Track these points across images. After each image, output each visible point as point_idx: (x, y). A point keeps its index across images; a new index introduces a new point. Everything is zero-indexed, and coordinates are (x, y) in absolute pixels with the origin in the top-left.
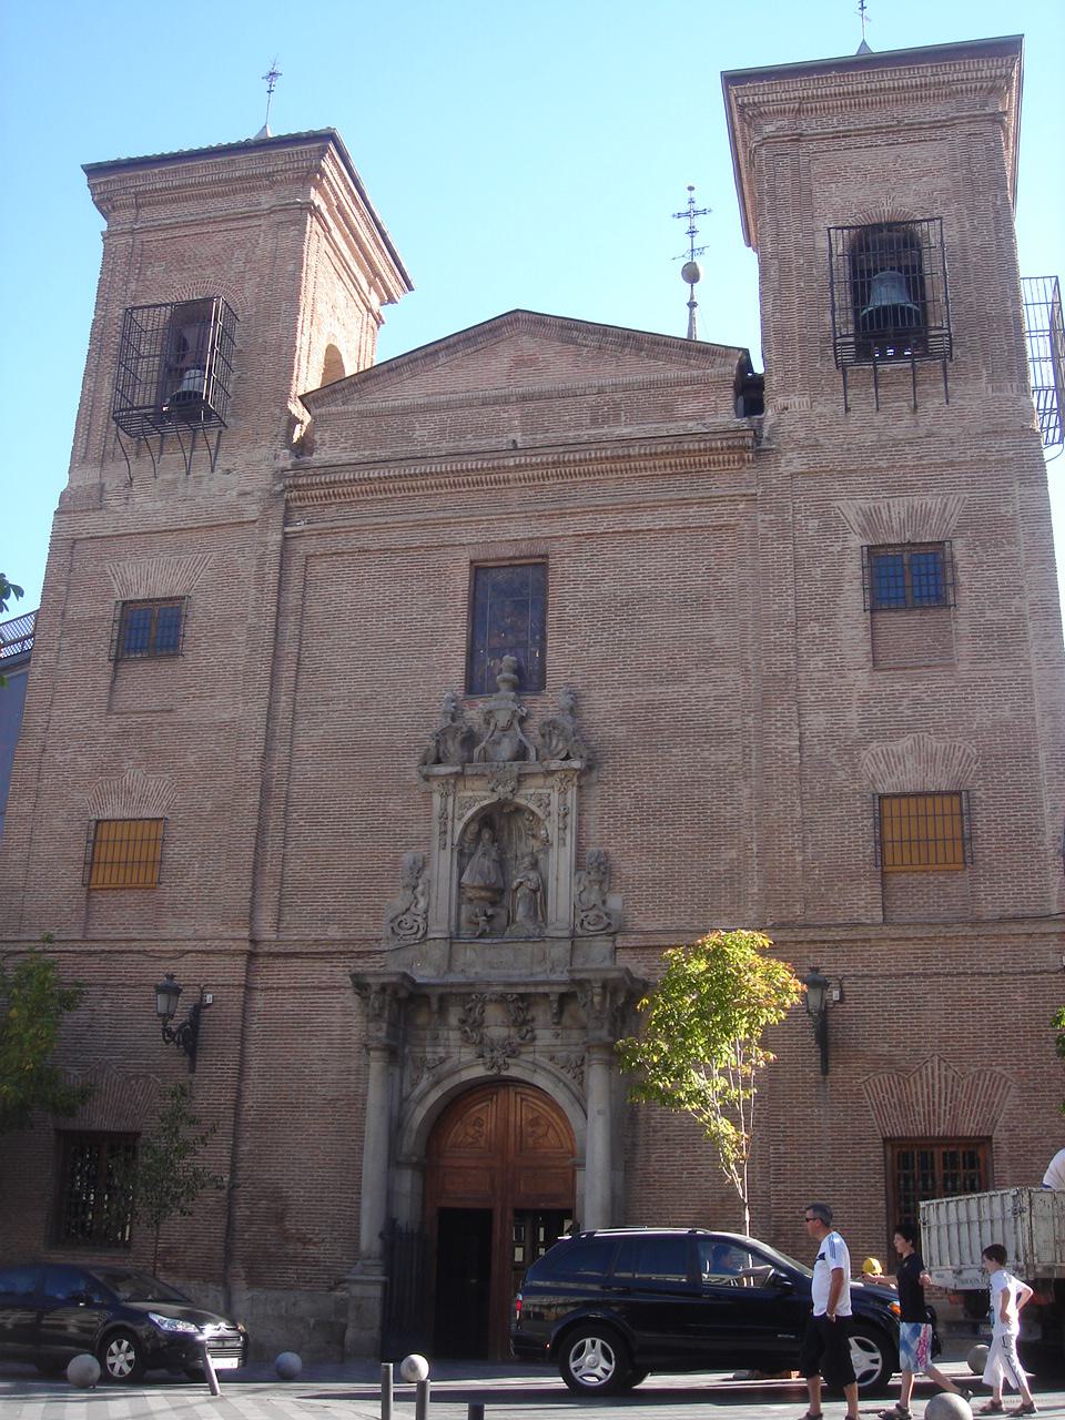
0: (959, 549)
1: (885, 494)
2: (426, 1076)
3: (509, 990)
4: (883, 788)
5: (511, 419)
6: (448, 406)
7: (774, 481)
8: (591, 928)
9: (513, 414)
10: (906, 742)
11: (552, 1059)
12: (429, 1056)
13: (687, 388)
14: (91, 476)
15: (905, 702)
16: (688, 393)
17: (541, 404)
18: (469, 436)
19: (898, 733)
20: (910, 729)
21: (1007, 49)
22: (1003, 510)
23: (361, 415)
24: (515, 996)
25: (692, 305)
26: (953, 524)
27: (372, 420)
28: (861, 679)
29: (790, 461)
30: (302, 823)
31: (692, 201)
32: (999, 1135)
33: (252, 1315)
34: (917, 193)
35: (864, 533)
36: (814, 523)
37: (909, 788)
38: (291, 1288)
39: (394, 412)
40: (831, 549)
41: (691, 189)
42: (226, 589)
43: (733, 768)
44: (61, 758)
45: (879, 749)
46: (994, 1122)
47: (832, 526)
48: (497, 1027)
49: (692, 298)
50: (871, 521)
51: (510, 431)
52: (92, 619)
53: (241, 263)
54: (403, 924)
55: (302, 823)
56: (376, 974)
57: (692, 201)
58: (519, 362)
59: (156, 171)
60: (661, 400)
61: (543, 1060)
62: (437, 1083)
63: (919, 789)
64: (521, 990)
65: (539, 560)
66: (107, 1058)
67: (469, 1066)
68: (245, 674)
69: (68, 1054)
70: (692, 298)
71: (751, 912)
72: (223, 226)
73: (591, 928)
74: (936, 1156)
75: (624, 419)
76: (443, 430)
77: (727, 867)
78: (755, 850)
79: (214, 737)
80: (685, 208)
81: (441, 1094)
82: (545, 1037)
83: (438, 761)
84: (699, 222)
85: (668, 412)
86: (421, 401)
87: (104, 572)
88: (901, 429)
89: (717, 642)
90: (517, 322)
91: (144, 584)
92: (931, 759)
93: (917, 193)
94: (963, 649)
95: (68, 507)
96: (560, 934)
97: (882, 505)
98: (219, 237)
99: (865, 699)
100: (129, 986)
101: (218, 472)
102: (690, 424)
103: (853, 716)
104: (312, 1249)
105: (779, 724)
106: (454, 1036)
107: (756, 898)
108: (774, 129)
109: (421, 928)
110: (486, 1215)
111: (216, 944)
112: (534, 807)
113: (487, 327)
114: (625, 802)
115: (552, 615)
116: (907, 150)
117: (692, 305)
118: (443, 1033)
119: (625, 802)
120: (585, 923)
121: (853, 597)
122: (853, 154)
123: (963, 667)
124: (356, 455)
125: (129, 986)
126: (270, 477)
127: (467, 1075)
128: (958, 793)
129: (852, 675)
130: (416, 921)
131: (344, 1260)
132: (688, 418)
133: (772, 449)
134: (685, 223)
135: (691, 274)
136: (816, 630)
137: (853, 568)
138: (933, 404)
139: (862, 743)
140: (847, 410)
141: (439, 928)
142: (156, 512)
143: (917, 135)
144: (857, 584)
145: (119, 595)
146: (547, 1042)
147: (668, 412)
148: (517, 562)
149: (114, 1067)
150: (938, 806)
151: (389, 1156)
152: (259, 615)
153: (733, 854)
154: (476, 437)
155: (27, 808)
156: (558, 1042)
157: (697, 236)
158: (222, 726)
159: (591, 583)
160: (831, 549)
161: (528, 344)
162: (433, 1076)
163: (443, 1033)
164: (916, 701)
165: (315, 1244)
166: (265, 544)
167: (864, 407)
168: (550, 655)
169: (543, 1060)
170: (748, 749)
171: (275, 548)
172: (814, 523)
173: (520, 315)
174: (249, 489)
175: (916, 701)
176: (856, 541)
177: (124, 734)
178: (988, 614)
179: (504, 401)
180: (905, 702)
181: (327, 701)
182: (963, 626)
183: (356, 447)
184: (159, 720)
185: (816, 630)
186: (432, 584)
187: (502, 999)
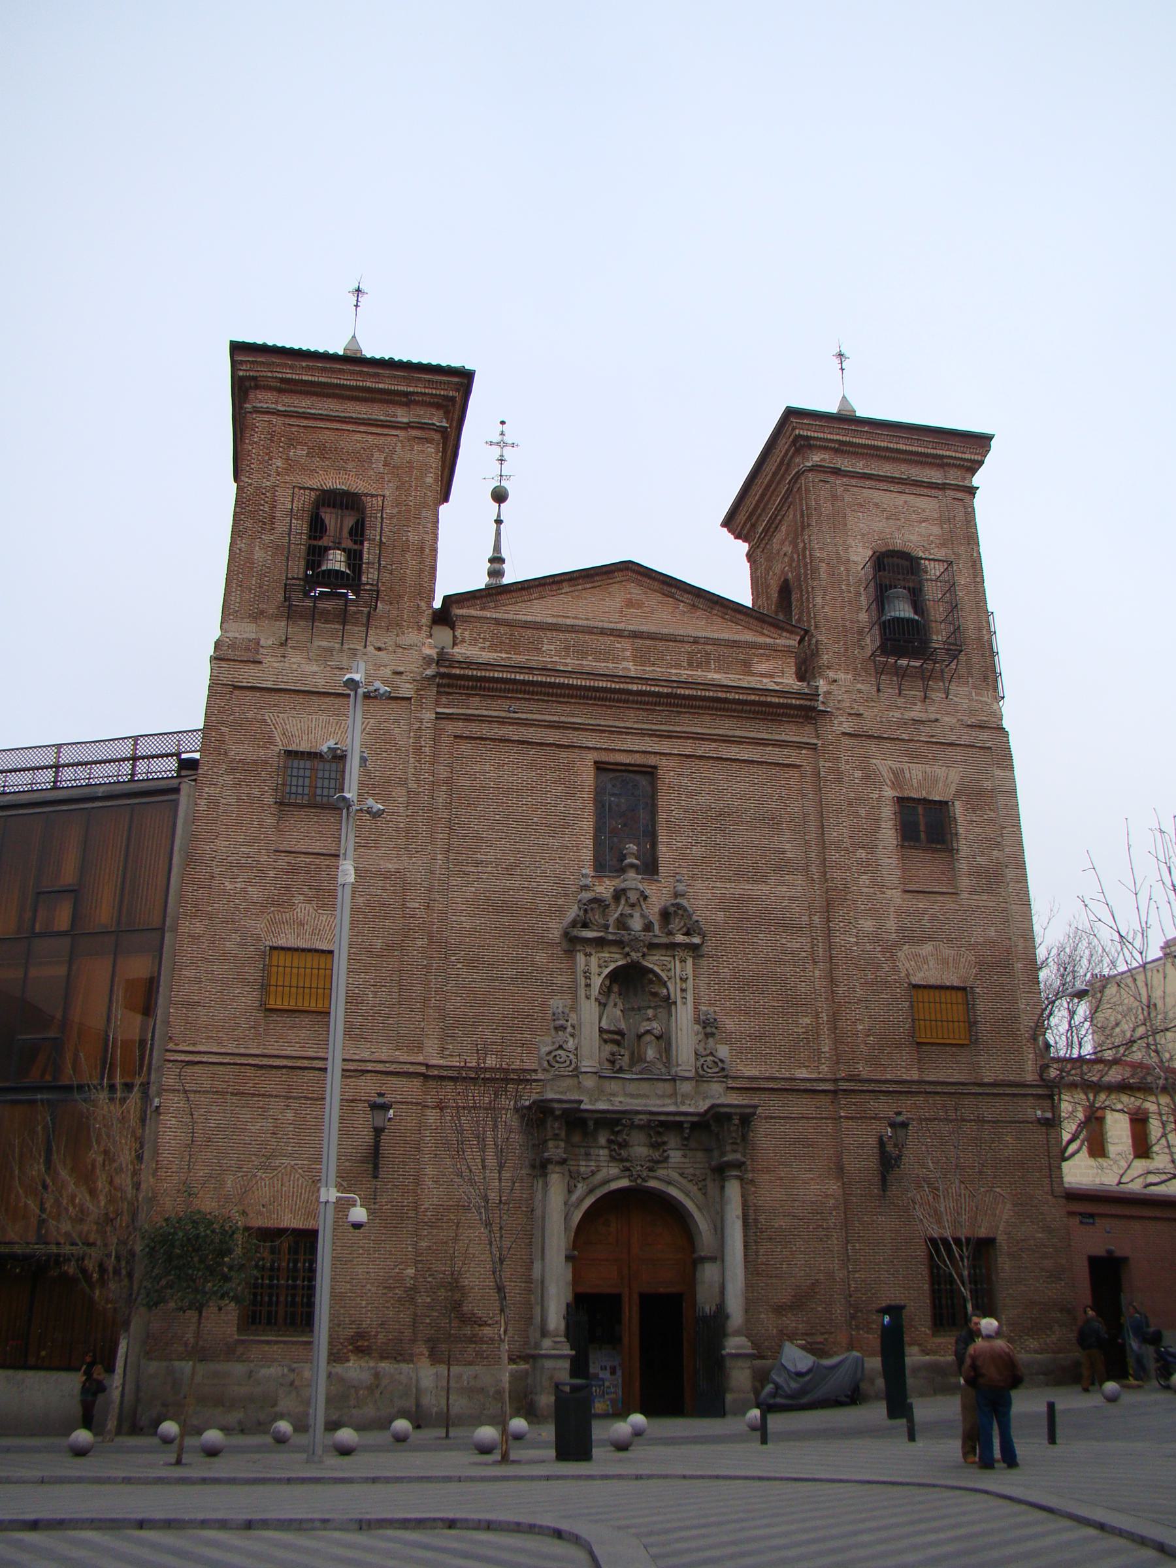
0: (958, 809)
1: (906, 759)
2: (580, 1185)
3: (653, 1118)
4: (915, 980)
5: (624, 650)
6: (571, 629)
7: (830, 737)
8: (709, 1071)
9: (625, 646)
10: (928, 948)
11: (681, 1175)
12: (582, 1169)
13: (762, 651)
14: (246, 631)
15: (926, 917)
16: (762, 655)
17: (648, 642)
18: (590, 658)
19: (921, 941)
20: (931, 939)
21: (982, 442)
22: (986, 784)
23: (498, 622)
24: (657, 1123)
25: (499, 522)
26: (953, 790)
27: (506, 628)
28: (895, 896)
29: (841, 723)
30: (459, 966)
31: (502, 434)
32: (1001, 1238)
33: (437, 1387)
34: (920, 535)
35: (893, 788)
36: (858, 774)
37: (932, 982)
38: (470, 1364)
39: (526, 625)
40: (871, 795)
41: (503, 423)
42: (384, 754)
43: (804, 954)
44: (232, 887)
45: (910, 950)
46: (997, 1227)
47: (871, 778)
48: (640, 1150)
49: (499, 515)
50: (898, 779)
51: (624, 659)
52: (255, 762)
53: (380, 465)
54: (558, 1058)
55: (459, 966)
56: (560, 1101)
57: (502, 434)
58: (630, 604)
59: (304, 364)
60: (742, 657)
61: (675, 1175)
62: (591, 1191)
63: (939, 983)
64: (662, 1118)
65: (649, 769)
66: (293, 1163)
67: (617, 1178)
68: (407, 832)
69: (253, 1158)
70: (499, 515)
71: (824, 1066)
72: (362, 429)
73: (709, 1071)
74: (263, 1312)
75: (713, 666)
76: (567, 649)
77: (804, 1030)
78: (825, 1019)
79: (380, 883)
80: (497, 438)
81: (593, 1200)
82: (675, 1156)
83: (585, 925)
84: (508, 452)
85: (746, 667)
86: (550, 620)
87: (264, 721)
88: (916, 712)
89: (789, 855)
90: (629, 570)
91: (305, 737)
92: (945, 962)
93: (920, 535)
94: (964, 882)
95: (222, 656)
96: (687, 1074)
97: (905, 766)
98: (358, 437)
99: (899, 912)
100: (311, 1099)
101: (370, 649)
102: (765, 680)
103: (891, 924)
104: (487, 1331)
105: (842, 924)
106: (604, 1152)
107: (827, 1055)
108: (819, 459)
109: (573, 1063)
110: (618, 1297)
111: (393, 1067)
112: (656, 969)
113: (604, 570)
114: (726, 972)
115: (662, 816)
116: (911, 498)
117: (499, 522)
118: (593, 1151)
119: (726, 972)
120: (705, 1067)
121: (888, 835)
122: (877, 493)
123: (964, 895)
124: (495, 655)
125: (311, 1099)
126: (420, 662)
127: (614, 1186)
128: (964, 989)
129: (889, 892)
130: (568, 1056)
131: (516, 1339)
132: (762, 675)
133: (827, 712)
134: (496, 451)
135: (499, 496)
136: (863, 856)
137: (888, 812)
138: (938, 696)
139: (897, 944)
140: (878, 690)
141: (588, 1064)
142: (314, 674)
143: (919, 490)
144: (890, 824)
145: (280, 744)
146: (678, 1160)
147: (746, 667)
148: (631, 768)
149: (300, 1171)
150: (948, 997)
151: (694, 1244)
152: (418, 781)
153: (807, 1020)
154: (595, 660)
155: (198, 927)
156: (687, 1160)
157: (505, 464)
158: (386, 875)
159: (691, 794)
160: (871, 795)
161: (635, 591)
162: (587, 1185)
163: (593, 1151)
164: (934, 918)
165: (489, 1325)
166: (421, 721)
167: (890, 690)
168: (662, 849)
169: (675, 1175)
170: (815, 941)
171: (429, 725)
172: (858, 774)
173: (630, 565)
174: (401, 669)
175: (934, 918)
176: (889, 793)
177: (293, 871)
178: (978, 859)
179: (618, 634)
180: (926, 917)
181: (478, 863)
182: (963, 866)
183: (492, 648)
184: (327, 863)
185: (863, 856)
186: (562, 776)
187: (646, 1128)
